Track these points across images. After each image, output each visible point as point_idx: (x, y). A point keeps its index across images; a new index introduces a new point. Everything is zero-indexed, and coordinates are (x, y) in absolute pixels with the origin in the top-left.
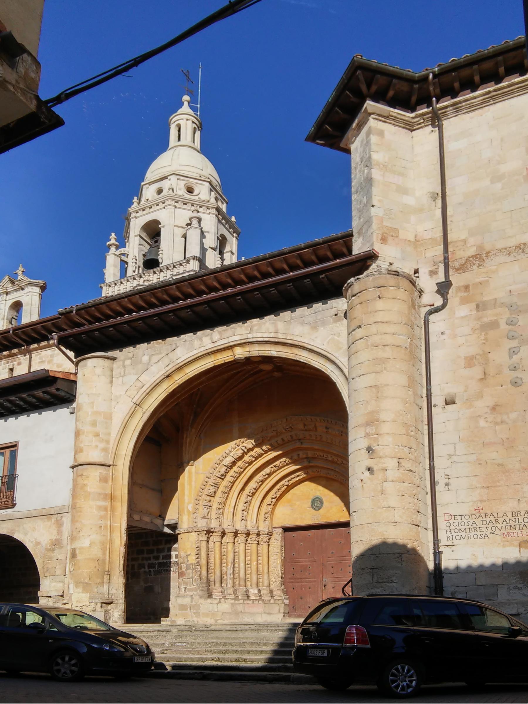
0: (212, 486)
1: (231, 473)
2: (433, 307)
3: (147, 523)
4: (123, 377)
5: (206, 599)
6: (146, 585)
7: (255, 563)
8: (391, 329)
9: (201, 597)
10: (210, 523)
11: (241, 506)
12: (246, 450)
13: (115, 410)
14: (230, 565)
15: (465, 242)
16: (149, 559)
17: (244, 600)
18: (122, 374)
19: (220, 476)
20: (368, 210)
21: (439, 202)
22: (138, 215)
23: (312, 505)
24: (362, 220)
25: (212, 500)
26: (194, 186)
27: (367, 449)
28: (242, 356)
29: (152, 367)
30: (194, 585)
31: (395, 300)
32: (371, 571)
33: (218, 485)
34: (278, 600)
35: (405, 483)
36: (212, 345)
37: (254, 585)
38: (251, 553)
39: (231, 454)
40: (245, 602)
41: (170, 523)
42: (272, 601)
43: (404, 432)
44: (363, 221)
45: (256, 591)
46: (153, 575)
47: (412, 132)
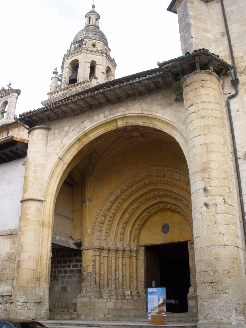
0: (103, 216)
1: (114, 207)
2: (230, 95)
3: (63, 242)
4: (53, 140)
5: (98, 299)
6: (62, 286)
7: (128, 272)
8: (212, 106)
9: (95, 297)
10: (102, 242)
11: (120, 231)
12: (123, 191)
13: (48, 163)
14: (113, 274)
15: (243, 58)
16: (64, 267)
17: (122, 299)
18: (53, 139)
19: (107, 209)
20: (189, 40)
21: (226, 37)
22: (68, 57)
23: (162, 230)
24: (186, 45)
25: (103, 226)
26: (96, 43)
27: (204, 190)
28: (122, 126)
29: (70, 134)
30: (91, 288)
31: (211, 88)
32: (211, 284)
33: (106, 215)
34: (143, 299)
35: (229, 215)
36: (104, 119)
37: (128, 288)
38: (126, 264)
39: (114, 194)
40: (123, 301)
41: (77, 242)
42: (139, 300)
43: (225, 176)
44: (187, 46)
45: (129, 293)
46: (66, 279)
47: (207, 3)
